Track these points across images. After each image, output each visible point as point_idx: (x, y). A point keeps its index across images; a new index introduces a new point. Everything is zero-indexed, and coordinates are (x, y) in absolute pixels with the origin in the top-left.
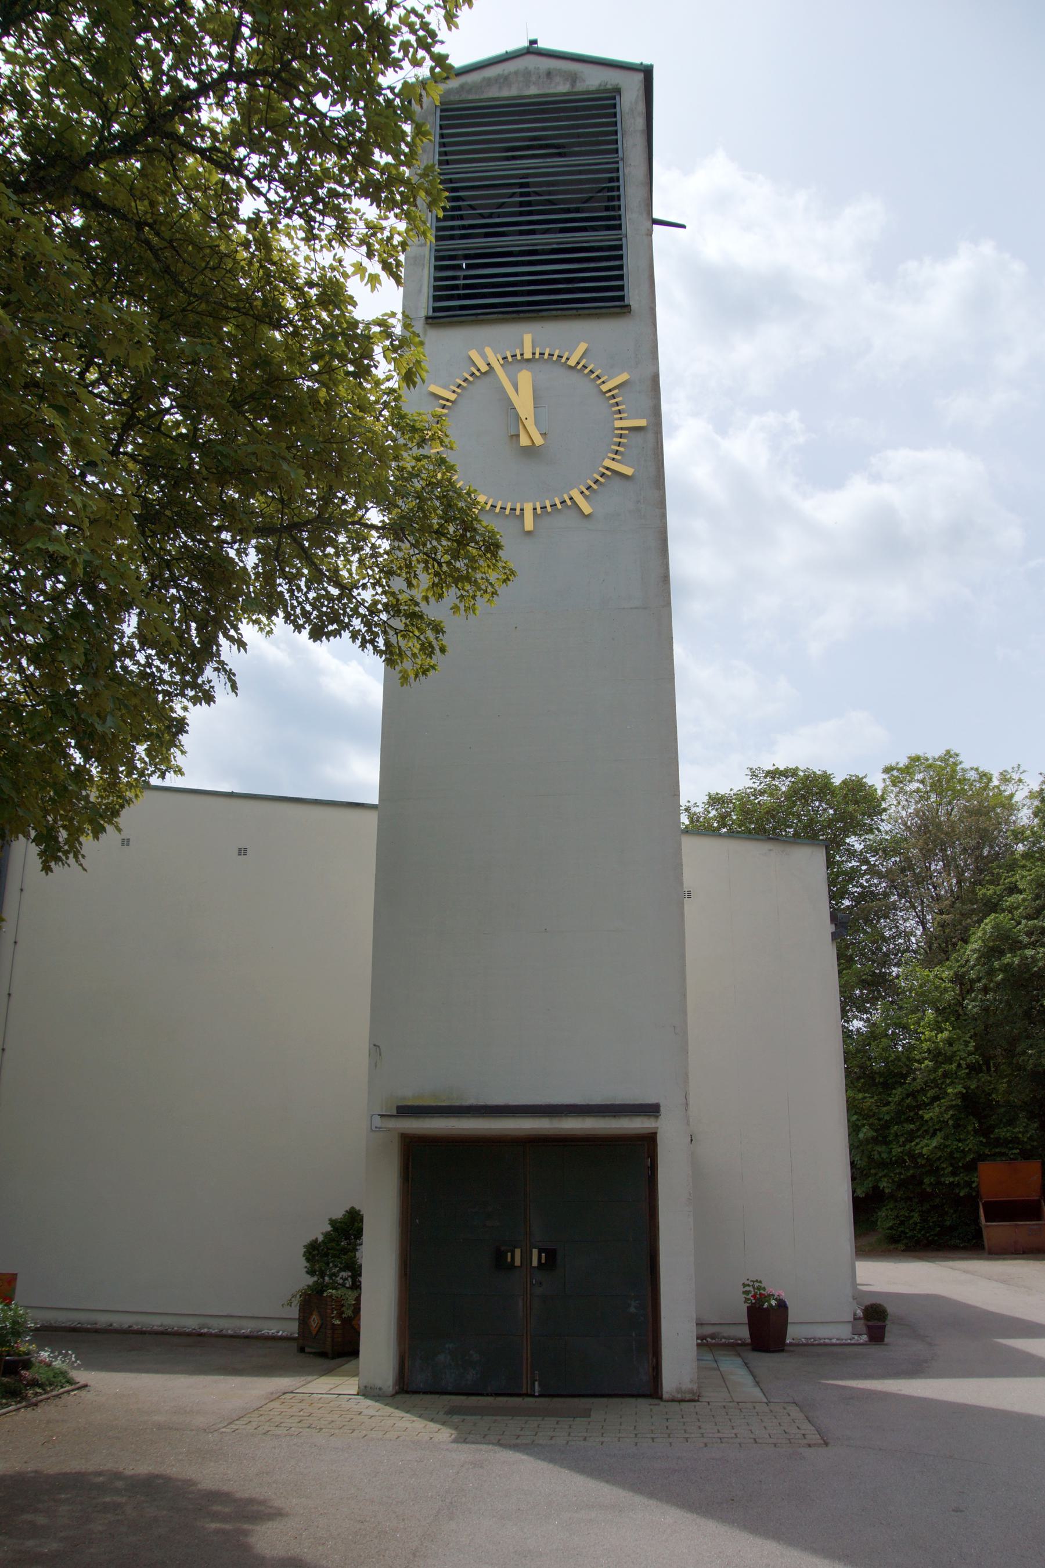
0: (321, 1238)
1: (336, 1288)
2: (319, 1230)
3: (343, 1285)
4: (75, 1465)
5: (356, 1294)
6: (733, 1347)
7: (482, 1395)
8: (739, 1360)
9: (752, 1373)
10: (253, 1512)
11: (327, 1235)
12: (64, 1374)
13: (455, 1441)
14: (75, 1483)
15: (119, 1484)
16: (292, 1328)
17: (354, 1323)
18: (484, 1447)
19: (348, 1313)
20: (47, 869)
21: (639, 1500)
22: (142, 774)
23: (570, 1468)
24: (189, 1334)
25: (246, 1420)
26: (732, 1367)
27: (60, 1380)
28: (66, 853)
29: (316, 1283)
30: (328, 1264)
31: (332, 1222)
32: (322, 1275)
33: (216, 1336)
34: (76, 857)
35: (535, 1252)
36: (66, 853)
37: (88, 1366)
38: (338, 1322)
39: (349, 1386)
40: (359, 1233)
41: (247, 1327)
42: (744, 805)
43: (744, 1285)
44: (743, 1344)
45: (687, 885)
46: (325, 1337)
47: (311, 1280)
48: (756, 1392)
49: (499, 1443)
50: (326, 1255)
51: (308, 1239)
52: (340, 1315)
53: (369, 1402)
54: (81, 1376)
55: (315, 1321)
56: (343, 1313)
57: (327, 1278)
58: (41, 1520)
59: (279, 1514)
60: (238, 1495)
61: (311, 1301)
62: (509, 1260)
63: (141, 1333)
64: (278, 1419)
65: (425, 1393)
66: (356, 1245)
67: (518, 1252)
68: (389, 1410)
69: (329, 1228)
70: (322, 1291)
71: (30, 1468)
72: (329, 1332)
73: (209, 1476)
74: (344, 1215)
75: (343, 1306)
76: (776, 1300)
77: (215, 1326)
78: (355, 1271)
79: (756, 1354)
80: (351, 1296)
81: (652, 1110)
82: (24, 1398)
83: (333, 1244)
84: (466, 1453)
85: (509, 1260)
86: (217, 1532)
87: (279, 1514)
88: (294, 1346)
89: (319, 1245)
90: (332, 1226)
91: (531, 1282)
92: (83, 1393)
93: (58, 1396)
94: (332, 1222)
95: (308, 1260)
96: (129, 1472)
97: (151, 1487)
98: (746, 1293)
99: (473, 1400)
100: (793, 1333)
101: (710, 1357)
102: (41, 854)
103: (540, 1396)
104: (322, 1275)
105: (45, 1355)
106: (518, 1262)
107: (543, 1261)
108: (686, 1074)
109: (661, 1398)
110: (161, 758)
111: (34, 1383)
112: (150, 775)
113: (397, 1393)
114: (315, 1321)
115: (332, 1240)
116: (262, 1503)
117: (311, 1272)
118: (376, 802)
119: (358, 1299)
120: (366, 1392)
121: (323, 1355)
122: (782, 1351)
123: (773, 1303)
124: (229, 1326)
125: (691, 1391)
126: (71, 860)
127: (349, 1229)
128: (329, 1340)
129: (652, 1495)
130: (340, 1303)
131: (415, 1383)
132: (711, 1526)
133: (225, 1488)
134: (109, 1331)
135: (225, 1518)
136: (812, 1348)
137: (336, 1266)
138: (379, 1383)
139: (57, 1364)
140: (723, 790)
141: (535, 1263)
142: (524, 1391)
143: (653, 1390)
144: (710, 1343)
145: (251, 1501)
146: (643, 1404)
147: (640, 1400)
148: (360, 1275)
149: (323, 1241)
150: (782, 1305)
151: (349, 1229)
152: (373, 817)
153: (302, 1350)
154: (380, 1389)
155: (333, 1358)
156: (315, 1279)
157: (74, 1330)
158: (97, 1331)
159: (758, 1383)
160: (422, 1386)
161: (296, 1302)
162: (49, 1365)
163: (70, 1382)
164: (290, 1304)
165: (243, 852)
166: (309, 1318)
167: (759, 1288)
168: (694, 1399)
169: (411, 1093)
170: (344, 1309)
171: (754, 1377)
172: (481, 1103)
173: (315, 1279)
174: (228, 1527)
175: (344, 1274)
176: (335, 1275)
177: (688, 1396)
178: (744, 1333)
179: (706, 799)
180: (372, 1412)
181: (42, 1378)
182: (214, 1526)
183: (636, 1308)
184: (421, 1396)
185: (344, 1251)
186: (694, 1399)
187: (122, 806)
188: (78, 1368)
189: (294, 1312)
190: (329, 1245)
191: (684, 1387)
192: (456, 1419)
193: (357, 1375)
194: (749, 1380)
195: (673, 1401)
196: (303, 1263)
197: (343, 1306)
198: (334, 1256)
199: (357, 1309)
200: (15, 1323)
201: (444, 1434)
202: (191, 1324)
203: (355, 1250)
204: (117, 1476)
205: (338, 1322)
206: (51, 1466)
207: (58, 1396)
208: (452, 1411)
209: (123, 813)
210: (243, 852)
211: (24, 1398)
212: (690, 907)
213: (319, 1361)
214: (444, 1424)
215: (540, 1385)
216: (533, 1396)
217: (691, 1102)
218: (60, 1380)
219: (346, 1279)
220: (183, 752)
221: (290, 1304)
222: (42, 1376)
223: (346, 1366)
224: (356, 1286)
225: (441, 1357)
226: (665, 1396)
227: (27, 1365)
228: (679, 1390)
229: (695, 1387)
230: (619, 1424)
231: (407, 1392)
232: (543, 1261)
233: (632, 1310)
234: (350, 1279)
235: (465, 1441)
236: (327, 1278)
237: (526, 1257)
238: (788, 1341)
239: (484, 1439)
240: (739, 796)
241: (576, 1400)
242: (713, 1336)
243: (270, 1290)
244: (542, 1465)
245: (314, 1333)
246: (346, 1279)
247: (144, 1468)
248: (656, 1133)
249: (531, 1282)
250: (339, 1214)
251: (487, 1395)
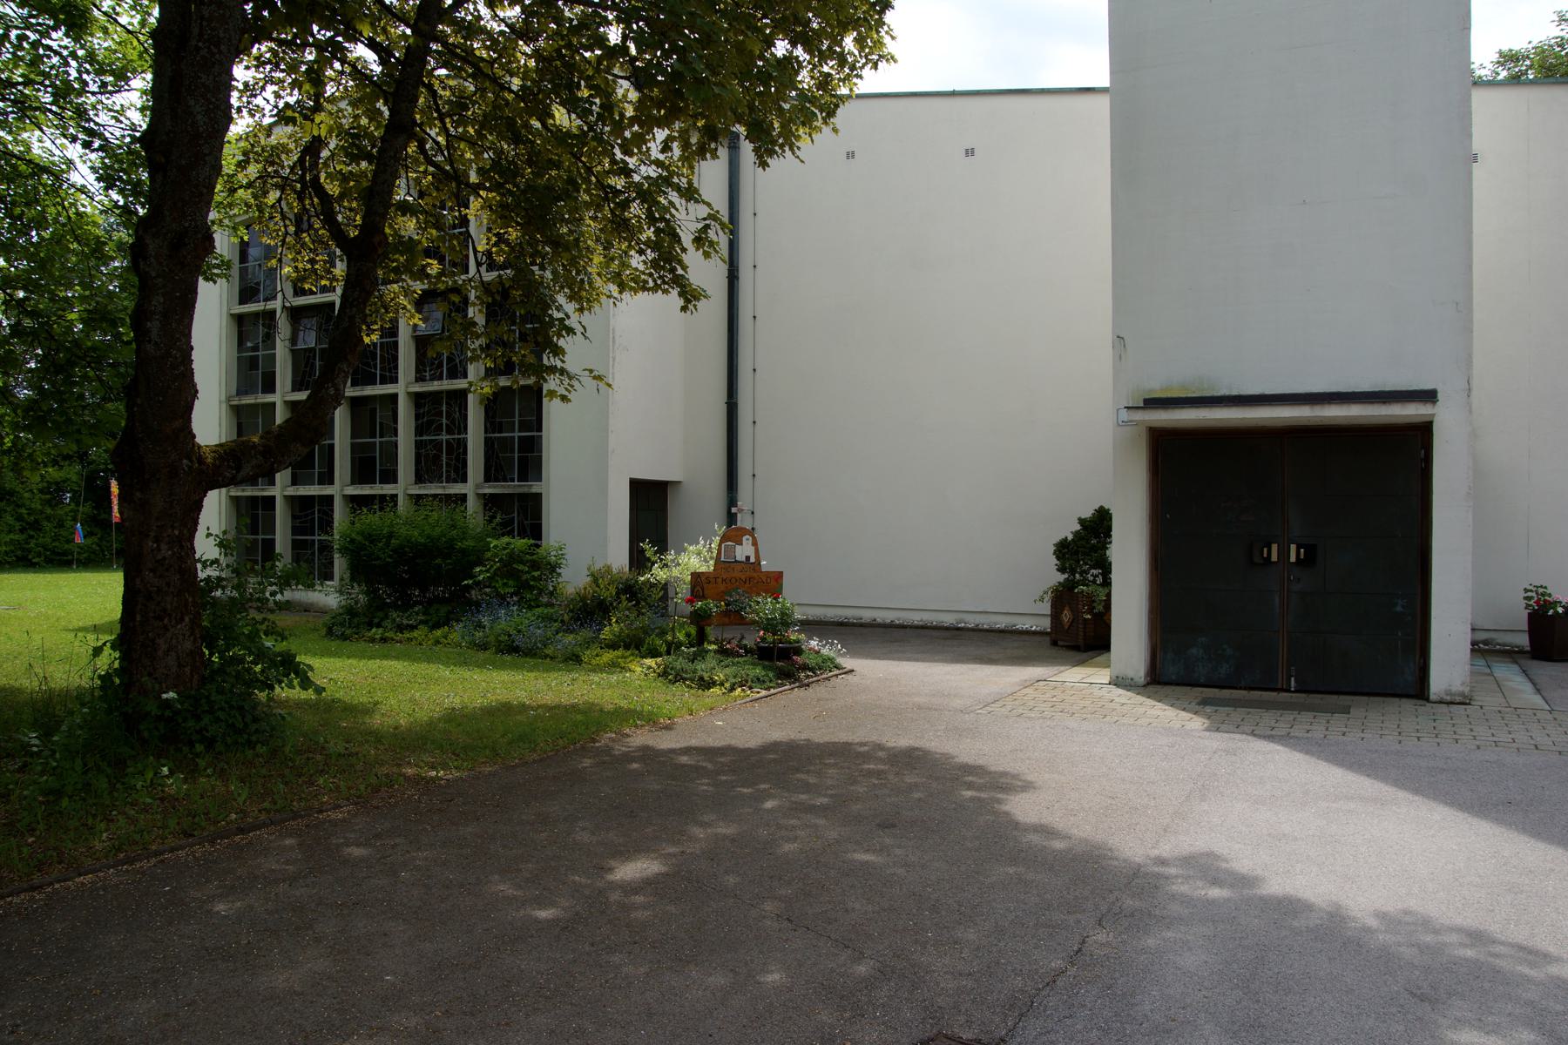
0: (1070, 537)
2: (1068, 529)
3: (1094, 582)
4: (842, 737)
6: (1510, 654)
8: (1515, 667)
9: (1531, 680)
10: (1004, 783)
11: (1076, 534)
12: (831, 660)
13: (1207, 730)
14: (841, 752)
15: (880, 754)
16: (1046, 624)
18: (1237, 736)
19: (1099, 608)
20: (764, 165)
21: (1402, 794)
22: (853, 68)
23: (1327, 760)
24: (947, 629)
25: (1000, 703)
26: (1510, 676)
27: (826, 666)
28: (782, 146)
31: (1081, 521)
32: (1073, 572)
33: (973, 630)
34: (791, 149)
35: (1293, 547)
36: (782, 146)
37: (853, 653)
39: (1101, 676)
41: (1002, 622)
42: (1544, 59)
43: (1526, 590)
44: (1521, 652)
45: (1477, 146)
46: (1077, 631)
47: (1061, 577)
48: (1538, 700)
49: (1253, 734)
50: (1077, 553)
51: (1057, 539)
53: (1120, 691)
54: (847, 662)
55: (1066, 616)
58: (812, 780)
59: (1027, 786)
60: (993, 769)
61: (1062, 597)
63: (902, 627)
64: (1031, 703)
65: (1178, 685)
67: (1274, 547)
68: (1141, 699)
69: (1078, 527)
71: (804, 736)
73: (966, 751)
77: (971, 621)
78: (1106, 568)
79: (1535, 662)
81: (1429, 396)
82: (797, 680)
84: (1217, 741)
86: (972, 799)
87: (1027, 786)
88: (1048, 639)
92: (849, 677)
93: (828, 679)
94: (1081, 521)
95: (1058, 558)
96: (890, 745)
97: (912, 759)
98: (1528, 598)
99: (1226, 693)
101: (1482, 662)
102: (756, 150)
103: (1296, 691)
104: (1073, 572)
105: (814, 643)
106: (1274, 558)
108: (1470, 356)
109: (1427, 699)
110: (875, 54)
111: (805, 667)
112: (862, 68)
114: (1066, 616)
115: (1081, 538)
116: (1015, 777)
117: (1061, 570)
118: (1106, 84)
119: (1109, 595)
120: (1118, 682)
121: (1076, 648)
123: (1560, 610)
124: (985, 622)
125: (1462, 694)
126: (788, 153)
127: (1098, 527)
129: (1417, 791)
130: (1090, 599)
131: (1166, 674)
132: (1485, 827)
133: (981, 762)
134: (873, 626)
135: (980, 788)
138: (1131, 673)
139: (825, 651)
140: (1519, 44)
141: (1293, 559)
144: (1484, 649)
145: (1004, 774)
146: (1407, 705)
147: (1404, 700)
151: (1098, 527)
152: (1104, 102)
153: (1054, 643)
157: (841, 624)
158: (862, 625)
159: (1538, 691)
161: (1047, 598)
162: (818, 652)
163: (837, 667)
164: (1042, 600)
165: (970, 152)
167: (1543, 594)
168: (1465, 702)
169: (1157, 386)
171: (1534, 684)
172: (1235, 393)
174: (983, 795)
175: (1095, 572)
177: (1458, 699)
178: (1523, 640)
179: (1495, 57)
180: (1123, 700)
181: (812, 662)
182: (969, 793)
186: (1465, 702)
187: (837, 106)
188: (844, 655)
189: (1046, 608)
191: (1454, 689)
192: (1208, 709)
194: (1528, 687)
196: (1053, 561)
200: (783, 614)
201: (1196, 723)
202: (948, 620)
204: (880, 747)
206: (820, 736)
207: (828, 679)
208: (1205, 702)
209: (839, 111)
210: (970, 152)
211: (797, 680)
212: (1478, 171)
213: (1071, 653)
214: (1196, 713)
216: (1288, 691)
217: (1475, 383)
218: (826, 666)
220: (893, 38)
221: (1042, 600)
222: (812, 661)
224: (1107, 583)
225: (1194, 651)
226: (1432, 697)
227: (799, 651)
228: (1448, 693)
229: (1467, 690)
230: (1383, 725)
231: (1159, 683)
233: (1399, 609)
235: (1218, 730)
237: (1284, 553)
239: (1238, 728)
240: (1541, 51)
242: (1486, 642)
243: (1025, 588)
244: (1298, 756)
247: (904, 742)
248: (1431, 423)
250: (1087, 513)
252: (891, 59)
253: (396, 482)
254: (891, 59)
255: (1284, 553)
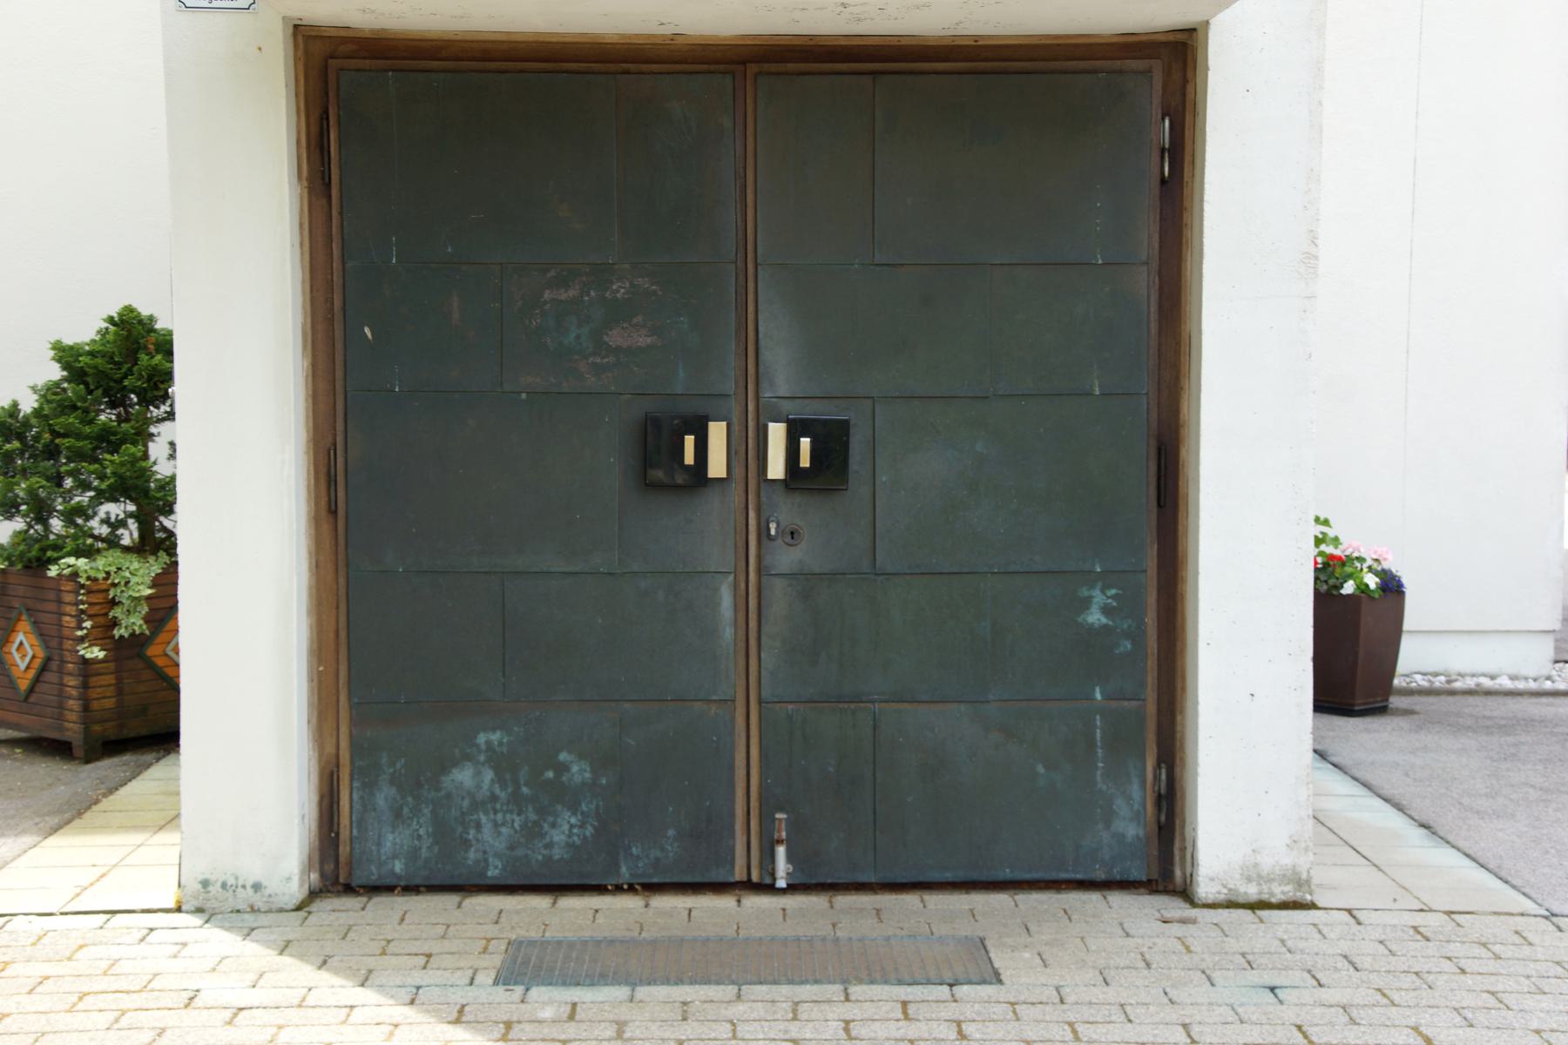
0: (28, 404)
1: (89, 553)
3: (112, 542)
5: (155, 567)
7: (600, 889)
11: (50, 393)
17: (152, 651)
19: (132, 623)
29: (21, 536)
30: (58, 480)
31: (66, 355)
32: (41, 512)
35: (777, 433)
38: (96, 653)
40: (158, 386)
51: (135, 306)
52: (104, 630)
56: (115, 623)
57: (56, 524)
62: (689, 458)
65: (411, 889)
66: (149, 422)
68: (297, 973)
69: (56, 373)
70: (44, 563)
72: (72, 681)
74: (104, 333)
75: (114, 603)
76: (1376, 573)
78: (153, 500)
80: (140, 576)
83: (72, 419)
85: (689, 458)
89: (26, 423)
90: (66, 366)
91: (763, 532)
94: (66, 355)
100: (1416, 658)
103: (792, 888)
104: (41, 512)
106: (717, 466)
107: (805, 462)
109: (1185, 893)
113: (314, 895)
119: (167, 583)
120: (210, 903)
121: (58, 749)
122: (1382, 710)
123: (1372, 581)
127: (124, 373)
128: (73, 704)
136: (1451, 698)
137: (85, 486)
138: (251, 867)
141: (776, 468)
142: (739, 874)
143: (1161, 867)
146: (1138, 914)
148: (169, 509)
149: (37, 413)
150: (1392, 587)
151: (124, 373)
154: (257, 887)
155: (88, 761)
156: (18, 524)
160: (398, 867)
166: (7, 641)
170: (117, 612)
173: (18, 524)
175: (113, 509)
176: (83, 512)
177: (1280, 892)
180: (224, 990)
183: (1106, 610)
184: (399, 903)
185: (108, 440)
190: (60, 422)
191: (1267, 862)
193: (171, 821)
195: (1231, 904)
197: (114, 603)
198: (77, 455)
199: (163, 607)
203: (143, 436)
205: (96, 653)
208: (525, 967)
213: (44, 770)
215: (790, 858)
216: (768, 888)
219: (122, 523)
223: (135, 786)
225: (463, 776)
226: (1205, 888)
229: (1303, 862)
231: (349, 890)
232: (805, 462)
233: (1095, 617)
234: (133, 525)
236: (56, 524)
237: (748, 451)
238: (1396, 682)
241: (911, 900)
245: (24, 685)
246: (122, 523)
249: (763, 532)
250: (85, 330)
251: (618, 889)
252: (34, 389)
253: (844, 426)
254: (34, 389)
255: (748, 451)
